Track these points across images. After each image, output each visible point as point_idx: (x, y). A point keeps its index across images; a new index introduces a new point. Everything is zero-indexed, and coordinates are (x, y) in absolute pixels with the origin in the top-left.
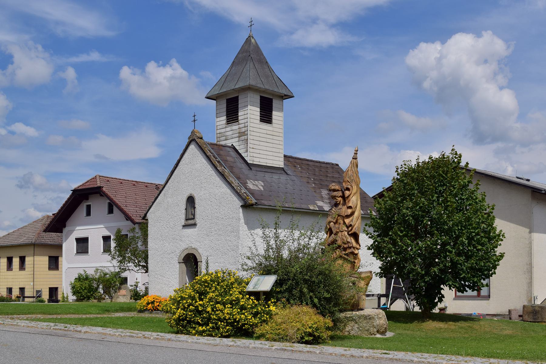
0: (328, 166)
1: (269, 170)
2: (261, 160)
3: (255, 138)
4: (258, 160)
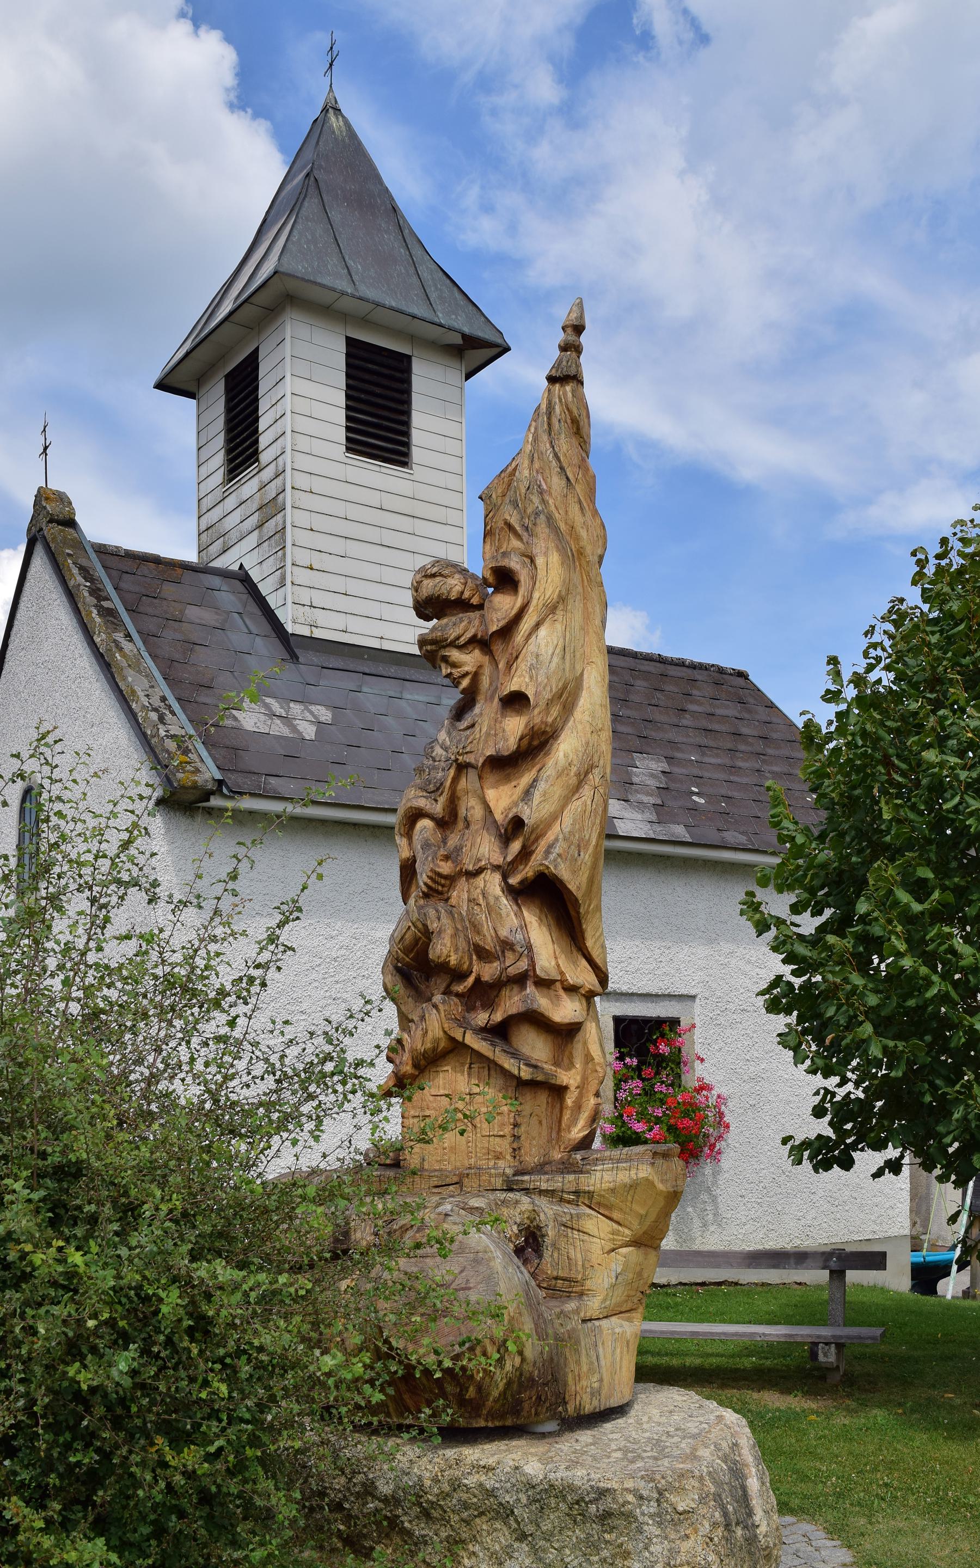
0: (697, 675)
1: (393, 670)
2: (355, 625)
3: (319, 523)
4: (338, 621)
